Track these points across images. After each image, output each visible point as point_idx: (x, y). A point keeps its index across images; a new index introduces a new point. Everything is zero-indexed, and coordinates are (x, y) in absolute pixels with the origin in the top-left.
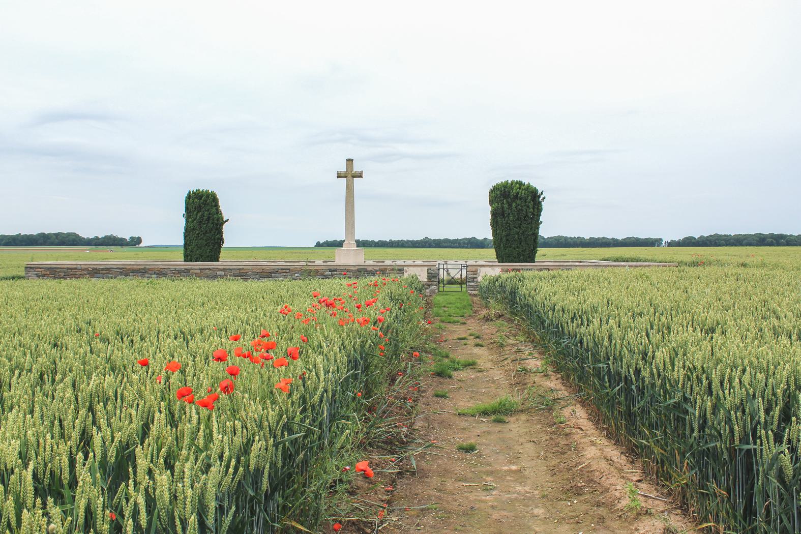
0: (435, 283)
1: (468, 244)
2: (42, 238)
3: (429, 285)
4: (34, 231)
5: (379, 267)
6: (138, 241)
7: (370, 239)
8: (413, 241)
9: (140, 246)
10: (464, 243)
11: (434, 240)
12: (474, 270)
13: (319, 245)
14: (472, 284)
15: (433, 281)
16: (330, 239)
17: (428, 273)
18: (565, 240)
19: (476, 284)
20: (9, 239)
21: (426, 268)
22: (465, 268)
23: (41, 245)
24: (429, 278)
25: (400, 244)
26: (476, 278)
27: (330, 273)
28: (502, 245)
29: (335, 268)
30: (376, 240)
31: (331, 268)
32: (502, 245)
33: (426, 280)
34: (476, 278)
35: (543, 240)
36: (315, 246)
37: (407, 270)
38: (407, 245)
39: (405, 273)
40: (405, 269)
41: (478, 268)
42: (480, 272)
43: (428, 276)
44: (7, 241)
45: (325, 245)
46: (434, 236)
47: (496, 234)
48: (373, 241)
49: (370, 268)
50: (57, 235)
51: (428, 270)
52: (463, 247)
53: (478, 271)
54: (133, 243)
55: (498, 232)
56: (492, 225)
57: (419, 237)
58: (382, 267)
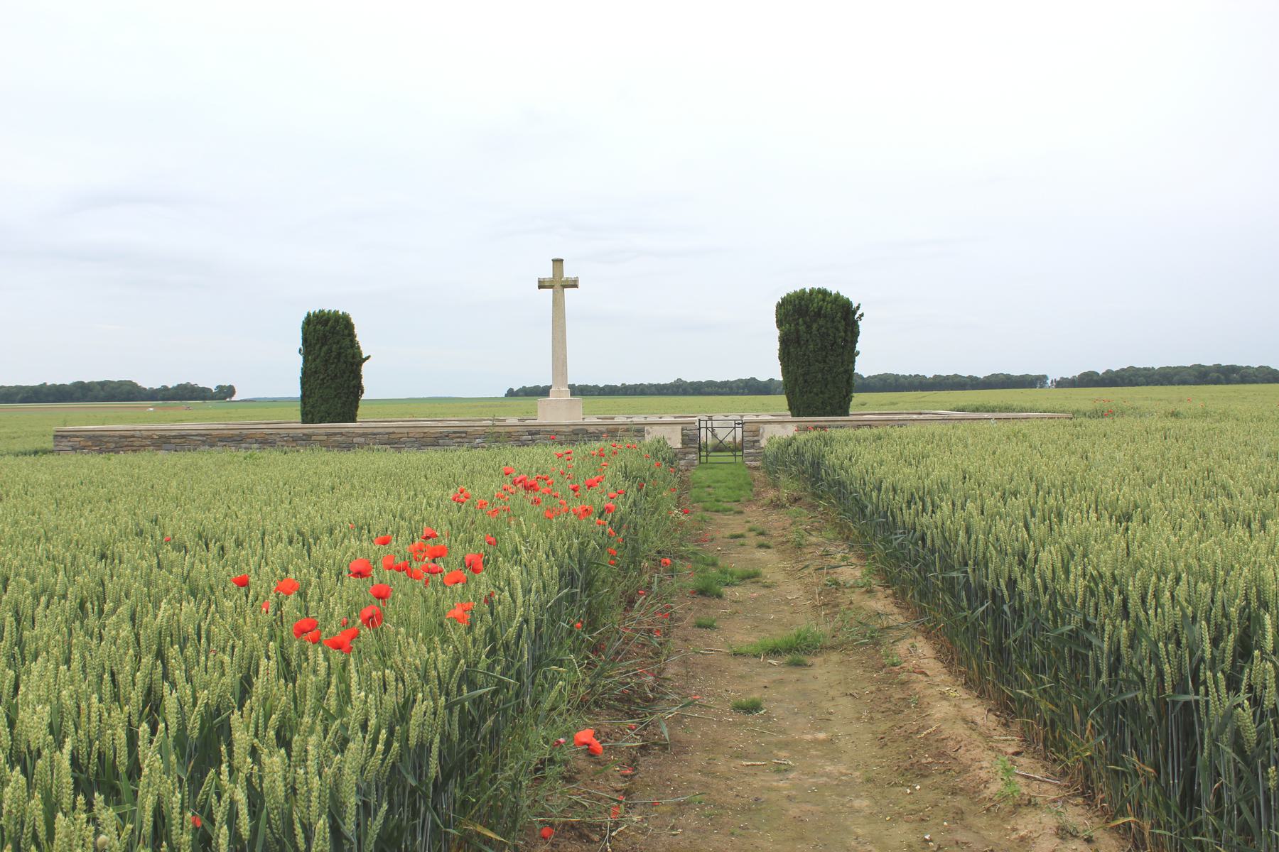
0: (694, 450)
1: (743, 388)
3: (685, 454)
4: (65, 378)
8: (659, 385)
9: (233, 399)
10: (738, 387)
12: (754, 429)
13: (511, 393)
14: (752, 451)
17: (683, 436)
18: (896, 381)
21: (680, 427)
23: (78, 400)
24: (683, 442)
25: (638, 390)
28: (797, 390)
29: (538, 428)
33: (679, 446)
34: (758, 441)
35: (860, 381)
36: (506, 395)
41: (761, 425)
42: (764, 432)
43: (683, 440)
44: (25, 395)
46: (689, 378)
47: (788, 372)
48: (596, 387)
49: (591, 429)
50: (103, 384)
51: (682, 430)
53: (761, 431)
55: (790, 369)
57: (667, 379)
58: (611, 427)
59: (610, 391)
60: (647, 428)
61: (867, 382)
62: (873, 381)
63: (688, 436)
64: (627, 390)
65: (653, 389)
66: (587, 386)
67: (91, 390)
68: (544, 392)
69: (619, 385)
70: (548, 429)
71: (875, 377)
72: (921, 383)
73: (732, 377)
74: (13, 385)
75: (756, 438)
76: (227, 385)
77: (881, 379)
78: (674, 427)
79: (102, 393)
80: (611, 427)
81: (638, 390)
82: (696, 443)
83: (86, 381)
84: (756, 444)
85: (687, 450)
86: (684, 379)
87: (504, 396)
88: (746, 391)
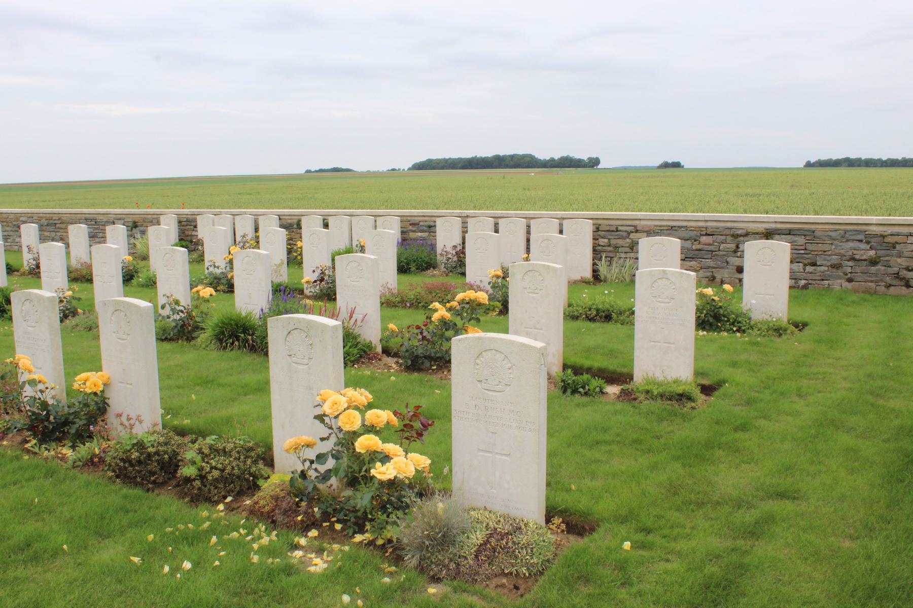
6: (677, 165)
9: (599, 167)
13: (809, 165)
16: (824, 157)
20: (464, 162)
23: (496, 167)
30: (884, 159)
36: (805, 166)
67: (504, 161)
76: (595, 157)
79: (512, 163)
83: (501, 154)
87: (802, 166)
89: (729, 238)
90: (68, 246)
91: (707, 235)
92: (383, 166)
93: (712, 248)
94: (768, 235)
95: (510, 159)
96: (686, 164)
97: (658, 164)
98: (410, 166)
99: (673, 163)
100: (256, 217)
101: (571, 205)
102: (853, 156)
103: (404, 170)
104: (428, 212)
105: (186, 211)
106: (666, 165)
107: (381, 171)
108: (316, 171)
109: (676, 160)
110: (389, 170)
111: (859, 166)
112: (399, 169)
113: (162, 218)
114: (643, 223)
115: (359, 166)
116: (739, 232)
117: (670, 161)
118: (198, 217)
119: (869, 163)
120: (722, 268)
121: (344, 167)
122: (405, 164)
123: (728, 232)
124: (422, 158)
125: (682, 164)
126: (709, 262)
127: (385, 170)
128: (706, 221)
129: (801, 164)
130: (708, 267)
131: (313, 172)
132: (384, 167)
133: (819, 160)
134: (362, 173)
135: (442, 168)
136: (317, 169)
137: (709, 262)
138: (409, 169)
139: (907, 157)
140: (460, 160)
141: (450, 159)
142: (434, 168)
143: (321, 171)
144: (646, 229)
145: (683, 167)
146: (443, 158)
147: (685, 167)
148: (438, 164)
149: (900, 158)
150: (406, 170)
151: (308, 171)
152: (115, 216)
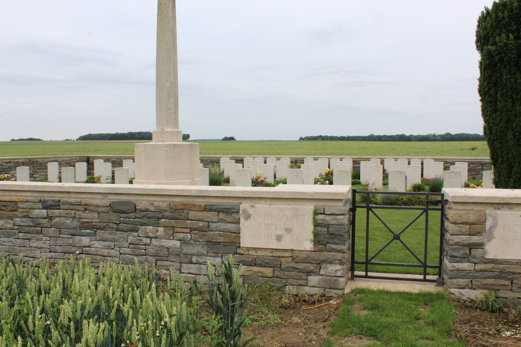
0: (339, 256)
1: (399, 138)
2: (130, 135)
3: (320, 263)
4: (125, 131)
5: (168, 199)
6: (232, 139)
7: (334, 135)
8: (363, 136)
9: (189, 139)
10: (397, 138)
11: (377, 136)
12: (472, 218)
13: (301, 139)
14: (465, 266)
15: (332, 250)
16: (309, 135)
17: (316, 225)
18: (466, 136)
19: (479, 267)
20: (111, 136)
21: (310, 208)
22: (439, 207)
23: (130, 139)
24: (317, 239)
25: (354, 138)
26: (480, 245)
27: (44, 212)
28: (510, 136)
29: (57, 197)
30: (339, 136)
31: (47, 197)
32: (510, 136)
33: (308, 246)
34: (480, 245)
35: (451, 136)
36: (299, 140)
37: (251, 211)
38: (359, 139)
39: (242, 220)
40: (242, 207)
41: (489, 211)
42: (494, 226)
43: (316, 235)
44: (110, 137)
45: (305, 139)
46: (376, 134)
47: (495, 110)
48: (336, 137)
49: (142, 204)
50: (139, 133)
51: (316, 213)
52: (396, 141)
53: (489, 224)
54: (185, 138)
55: (499, 105)
56: (484, 91)
57: (366, 134)
58: (178, 200)
59: (342, 139)
60: (245, 206)
61: (453, 136)
62: (456, 136)
63: (328, 226)
64: (349, 139)
65: (361, 138)
66: (333, 136)
67: (134, 135)
68: (147, 137)
69: (346, 136)
70: (73, 199)
71: (457, 134)
72: (477, 137)
73: (394, 134)
74: (106, 133)
75: (475, 239)
76: (187, 134)
77: (460, 136)
78: (299, 206)
79: (139, 136)
80: (178, 200)
81: (354, 138)
82: (343, 242)
83: (133, 132)
84: (476, 252)
85: (326, 255)
86: (373, 134)
87: (298, 140)
88: (400, 139)
89: (480, 165)
90: (75, 168)
91: (472, 164)
92: (61, 138)
93: (474, 168)
94: (54, 161)
95: (138, 134)
96: (237, 138)
97: (222, 139)
98: (78, 138)
99: (230, 137)
100: (409, 160)
101: (333, 154)
102: (323, 135)
103: (74, 140)
104: (302, 156)
105: (295, 156)
106: (226, 139)
107: (59, 140)
108: (18, 140)
109: (232, 136)
110: (64, 140)
111: (327, 140)
112: (71, 140)
113: (305, 160)
114: (449, 160)
115: (45, 138)
116: (484, 163)
117: (228, 136)
118: (244, 158)
119: (332, 138)
120: (477, 175)
121: (36, 138)
122: (75, 137)
123: (480, 163)
124: (85, 133)
125: (235, 138)
126: (473, 173)
127: (62, 140)
128: (472, 159)
129: (298, 139)
130: (473, 175)
131: (16, 140)
132: (61, 138)
133: (404, 135)
134: (47, 141)
135: (97, 139)
136: (19, 139)
137: (473, 173)
138: (77, 140)
139: (350, 136)
140: (108, 135)
141: (102, 134)
142: (92, 139)
143: (21, 140)
144: (451, 162)
145: (235, 140)
146: (98, 133)
147: (236, 140)
148: (95, 137)
149: (346, 136)
150: (75, 140)
151: (13, 140)
152: (70, 158)
